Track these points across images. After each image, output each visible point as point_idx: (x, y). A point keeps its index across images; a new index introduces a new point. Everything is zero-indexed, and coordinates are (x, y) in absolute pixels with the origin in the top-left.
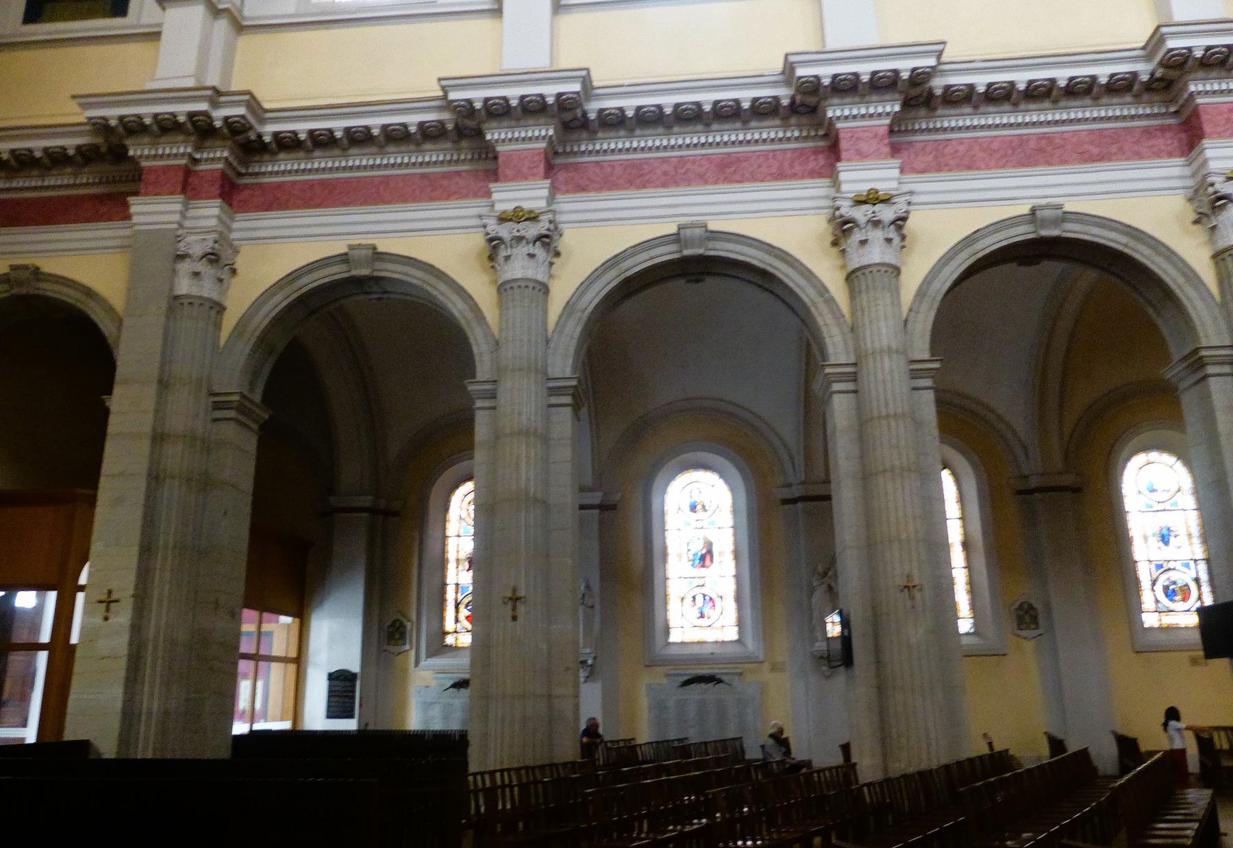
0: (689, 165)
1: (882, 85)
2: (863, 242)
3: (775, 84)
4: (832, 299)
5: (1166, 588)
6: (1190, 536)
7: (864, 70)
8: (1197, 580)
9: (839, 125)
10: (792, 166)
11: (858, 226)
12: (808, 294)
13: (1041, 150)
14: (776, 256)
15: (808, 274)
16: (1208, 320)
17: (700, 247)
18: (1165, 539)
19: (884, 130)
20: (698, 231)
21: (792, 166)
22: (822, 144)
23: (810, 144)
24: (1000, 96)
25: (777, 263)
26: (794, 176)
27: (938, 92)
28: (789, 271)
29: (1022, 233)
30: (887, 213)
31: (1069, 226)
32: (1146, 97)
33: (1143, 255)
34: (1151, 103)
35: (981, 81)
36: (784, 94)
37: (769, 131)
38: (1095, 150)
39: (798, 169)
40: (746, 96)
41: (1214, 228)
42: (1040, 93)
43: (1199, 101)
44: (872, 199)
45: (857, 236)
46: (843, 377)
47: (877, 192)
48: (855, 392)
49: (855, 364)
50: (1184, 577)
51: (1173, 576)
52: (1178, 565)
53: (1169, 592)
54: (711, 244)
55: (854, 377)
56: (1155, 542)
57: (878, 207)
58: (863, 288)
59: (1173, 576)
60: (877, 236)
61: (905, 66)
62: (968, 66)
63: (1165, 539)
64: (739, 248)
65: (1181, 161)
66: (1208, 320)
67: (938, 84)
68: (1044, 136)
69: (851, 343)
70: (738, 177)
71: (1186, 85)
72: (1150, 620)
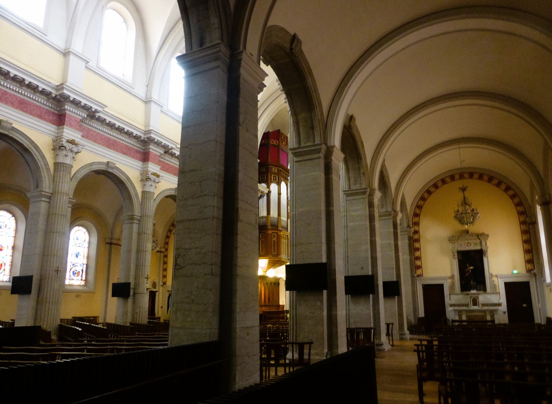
0: (8, 96)
1: (86, 108)
2: (66, 156)
3: (53, 88)
4: (49, 168)
5: (73, 272)
6: (84, 256)
7: (84, 102)
8: (82, 270)
9: (67, 112)
10: (45, 115)
11: (66, 149)
12: (41, 163)
13: (113, 145)
14: (33, 146)
15: (43, 157)
16: (137, 207)
17: (7, 131)
18: (77, 256)
19: (78, 120)
20: (9, 126)
21: (45, 115)
22: (56, 112)
23: (53, 111)
24: (111, 126)
25: (33, 148)
26: (44, 119)
27: (97, 117)
28: (37, 153)
29: (103, 167)
30: (75, 149)
31: (114, 170)
32: (51, 101)
33: (128, 185)
34: (140, 144)
35: (108, 119)
36: (54, 93)
37: (42, 99)
38: (125, 151)
39: (47, 117)
40: (42, 86)
41: (145, 185)
42: (120, 130)
43: (150, 150)
44: (72, 142)
45: (64, 152)
46: (46, 196)
47: (75, 141)
48: (49, 203)
49: (52, 194)
50: (79, 269)
51: (76, 268)
52: (78, 265)
53: (74, 273)
54: (11, 132)
55: (50, 198)
56: (74, 256)
57: (73, 146)
58: (62, 170)
59: (76, 268)
60: (70, 155)
61: (94, 107)
62: (107, 114)
63: (77, 256)
64: (21, 137)
65: (142, 163)
66: (137, 207)
67: (97, 115)
68: (114, 141)
69: (52, 186)
70: (25, 110)
71: (150, 145)
72: (67, 282)
